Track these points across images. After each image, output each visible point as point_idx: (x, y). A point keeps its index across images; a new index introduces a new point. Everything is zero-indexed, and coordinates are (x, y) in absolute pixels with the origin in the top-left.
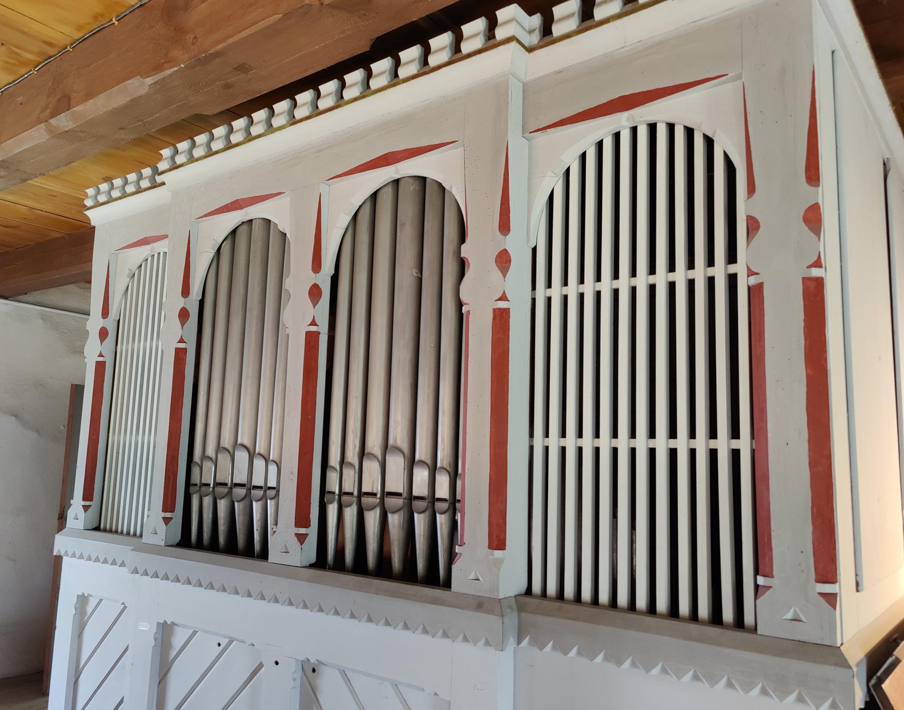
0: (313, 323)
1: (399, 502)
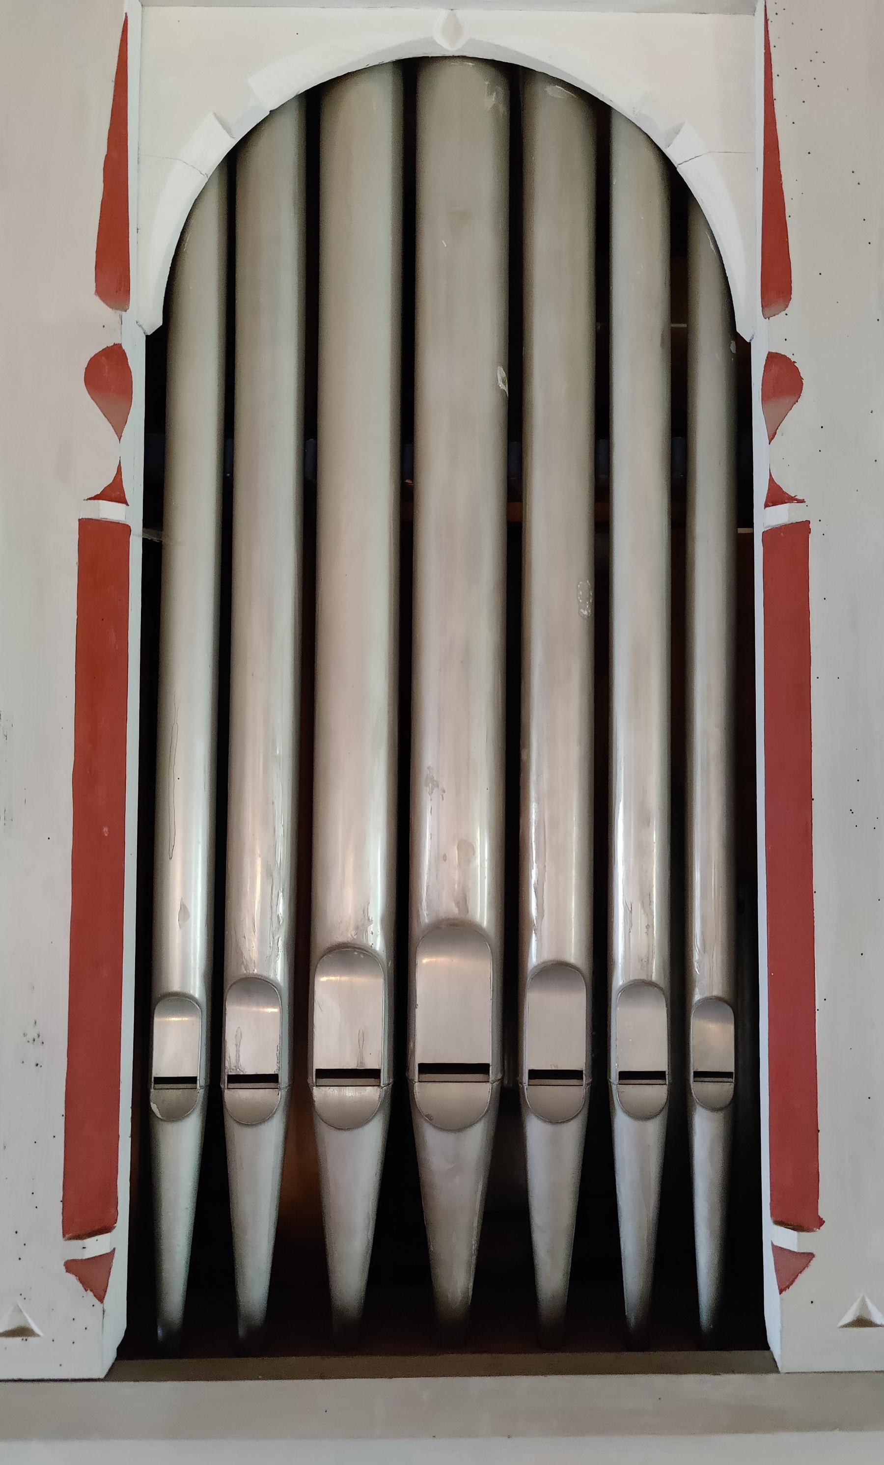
0: (114, 492)
1: (370, 1094)
